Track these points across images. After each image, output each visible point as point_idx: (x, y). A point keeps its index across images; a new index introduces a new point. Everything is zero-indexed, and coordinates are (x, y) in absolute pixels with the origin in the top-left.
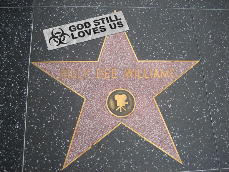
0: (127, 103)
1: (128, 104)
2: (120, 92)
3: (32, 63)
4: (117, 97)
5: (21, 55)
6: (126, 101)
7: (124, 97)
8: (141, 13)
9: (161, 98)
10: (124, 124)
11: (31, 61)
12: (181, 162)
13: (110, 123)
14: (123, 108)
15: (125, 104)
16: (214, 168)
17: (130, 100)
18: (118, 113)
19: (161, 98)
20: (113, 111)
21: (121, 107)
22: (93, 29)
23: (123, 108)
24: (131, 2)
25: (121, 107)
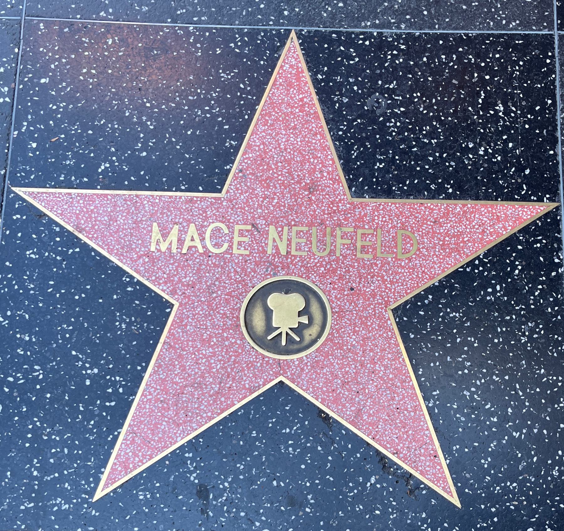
0: (305, 320)
1: (307, 322)
2: (258, 322)
3: (293, 31)
4: (274, 300)
5: (15, 218)
6: (300, 314)
7: (296, 301)
8: (509, 265)
10: (287, 382)
11: (295, 30)
14: (290, 332)
16: (78, 16)
18: (274, 346)
20: (259, 341)
21: (284, 330)
23: (290, 332)
24: (524, 263)
25: (284, 330)
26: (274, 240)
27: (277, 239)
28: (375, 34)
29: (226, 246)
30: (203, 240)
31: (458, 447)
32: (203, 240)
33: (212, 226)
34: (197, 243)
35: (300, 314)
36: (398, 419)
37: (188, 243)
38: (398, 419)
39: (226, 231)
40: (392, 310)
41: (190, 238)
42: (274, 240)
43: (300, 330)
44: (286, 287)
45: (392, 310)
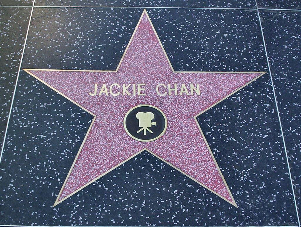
0: (155, 124)
4: (139, 115)
6: (152, 121)
7: (151, 115)
9: (201, 119)
12: (234, 203)
13: (134, 148)
15: (152, 125)
17: (159, 118)
18: (140, 136)
19: (201, 119)
26: (194, 90)
27: (195, 89)
28: (112, 9)
29: (166, 93)
30: (109, 90)
31: (64, 173)
32: (109, 90)
33: (114, 84)
34: (106, 92)
35: (152, 121)
36: (194, 159)
37: (182, 91)
38: (194, 159)
39: (119, 87)
40: (94, 117)
41: (193, 90)
42: (194, 90)
44: (145, 110)
45: (94, 117)
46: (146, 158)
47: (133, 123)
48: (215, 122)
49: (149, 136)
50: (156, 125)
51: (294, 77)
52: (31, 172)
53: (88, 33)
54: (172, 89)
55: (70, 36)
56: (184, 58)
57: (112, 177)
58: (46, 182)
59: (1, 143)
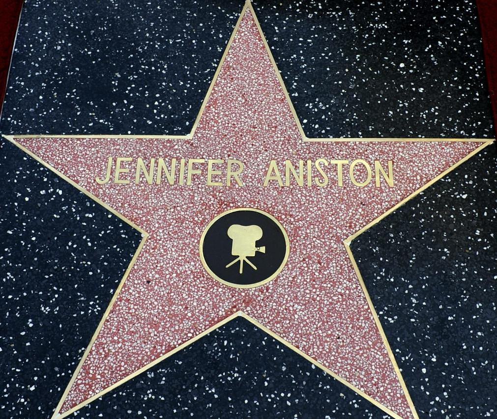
0: (263, 250)
1: (264, 247)
4: (234, 231)
6: (258, 244)
7: (256, 232)
18: (232, 275)
21: (242, 258)
22: (256, 247)
25: (242, 258)
42: (148, 171)
43: (257, 258)
44: (246, 218)
46: (240, 331)
47: (217, 248)
48: (388, 252)
49: (250, 277)
50: (264, 247)
51: (302, 55)
52: (77, 217)
53: (147, 92)
54: (303, 173)
55: (17, 198)
56: (332, 105)
57: (168, 104)
58: (88, 240)
59: (87, 128)
